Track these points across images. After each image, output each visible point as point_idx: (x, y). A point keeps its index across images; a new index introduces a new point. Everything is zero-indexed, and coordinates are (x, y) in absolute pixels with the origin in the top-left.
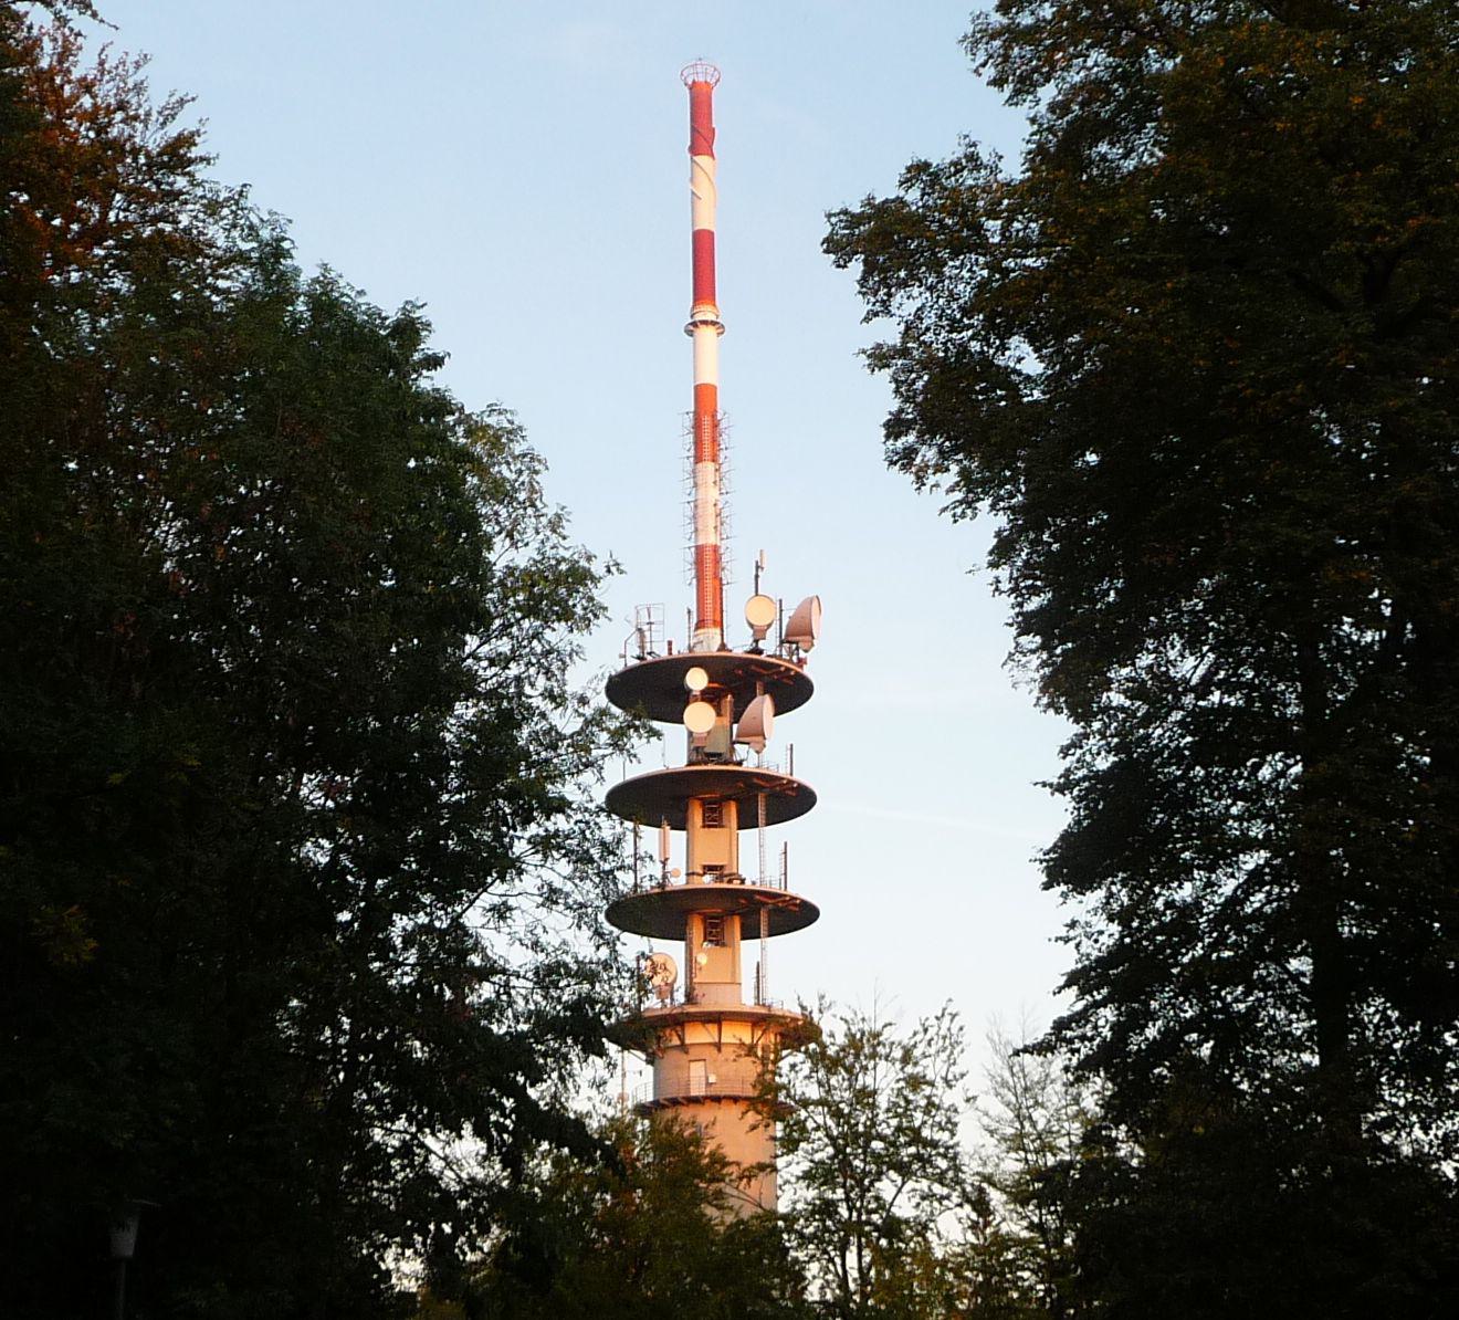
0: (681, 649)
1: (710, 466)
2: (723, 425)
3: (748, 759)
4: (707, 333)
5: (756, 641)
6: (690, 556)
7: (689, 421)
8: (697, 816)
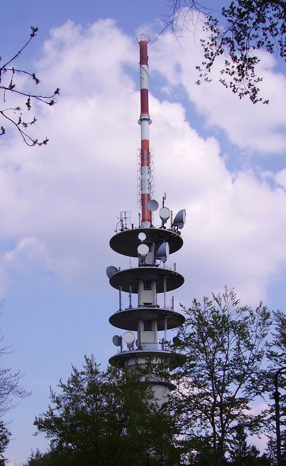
0: (136, 226)
1: (147, 167)
2: (151, 154)
3: (161, 264)
4: (146, 123)
5: (163, 224)
6: (139, 197)
7: (139, 152)
8: (142, 326)
